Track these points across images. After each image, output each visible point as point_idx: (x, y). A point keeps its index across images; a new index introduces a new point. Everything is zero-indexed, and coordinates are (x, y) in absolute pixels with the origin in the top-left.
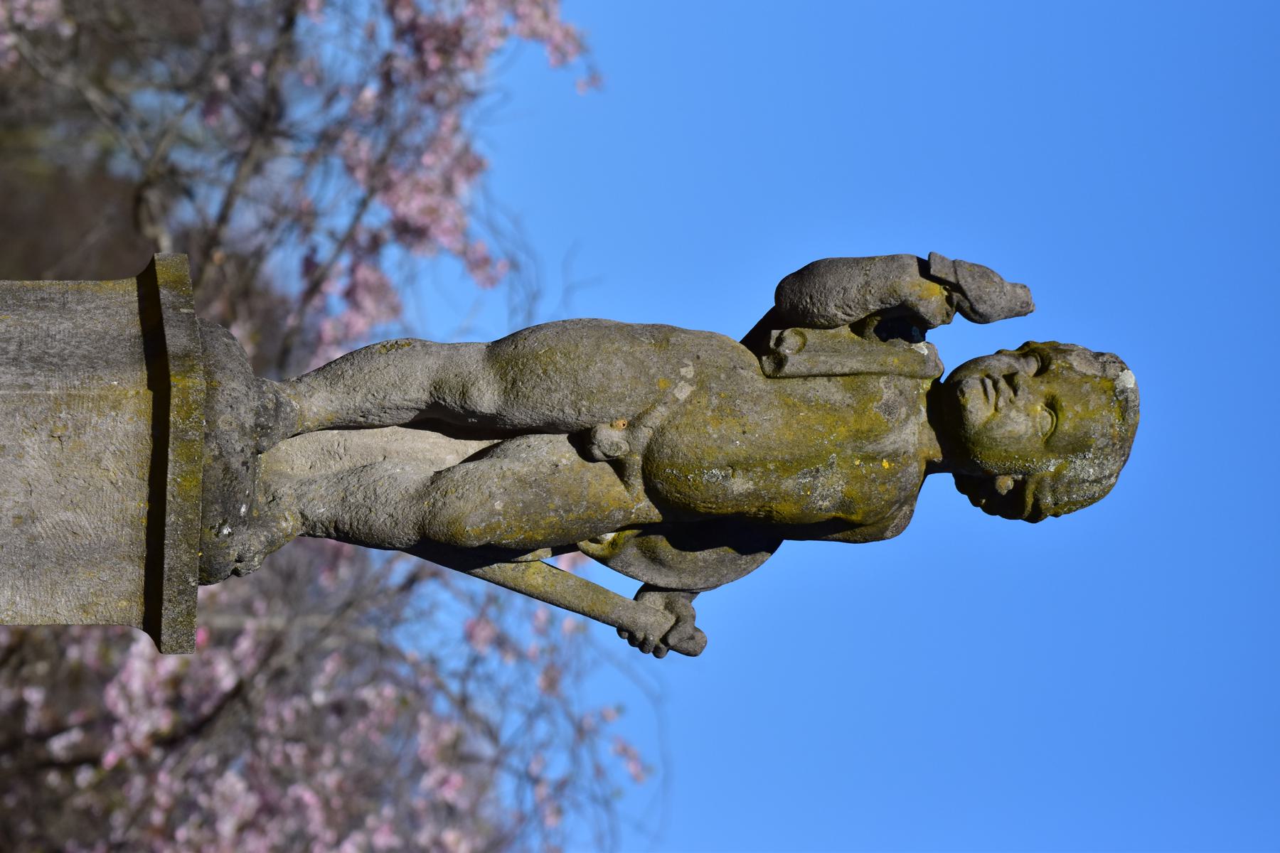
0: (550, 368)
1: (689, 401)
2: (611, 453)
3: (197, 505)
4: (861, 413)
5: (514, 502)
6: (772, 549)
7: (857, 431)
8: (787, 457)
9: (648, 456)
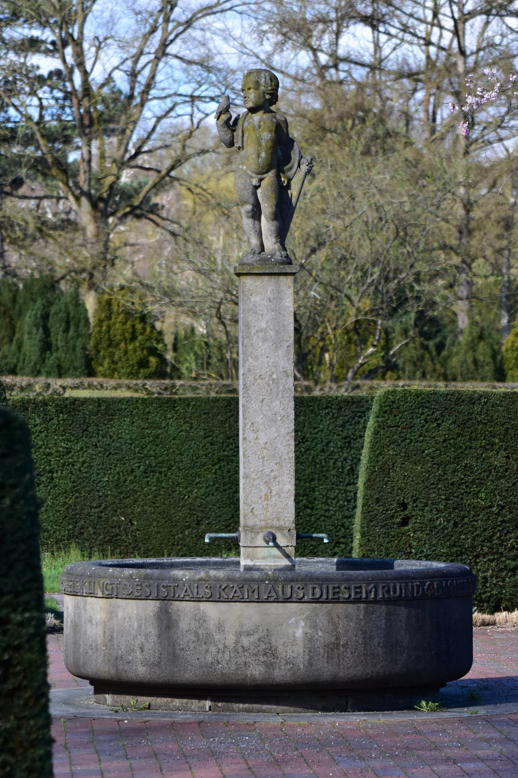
6: (292, 141)
9: (258, 174)
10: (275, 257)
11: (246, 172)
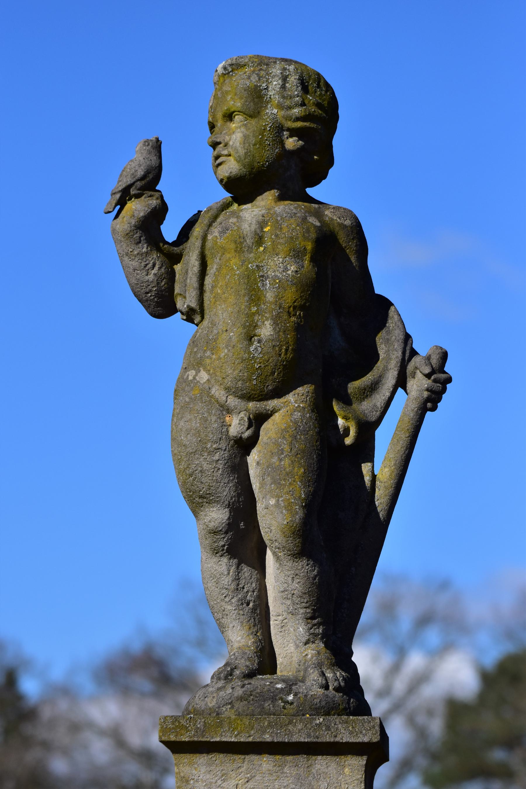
0: (188, 472)
1: (208, 371)
2: (246, 424)
3: (257, 719)
4: (224, 250)
5: (270, 491)
6: (380, 309)
7: (236, 251)
8: (246, 298)
9: (248, 397)
10: (302, 688)
11: (206, 392)
